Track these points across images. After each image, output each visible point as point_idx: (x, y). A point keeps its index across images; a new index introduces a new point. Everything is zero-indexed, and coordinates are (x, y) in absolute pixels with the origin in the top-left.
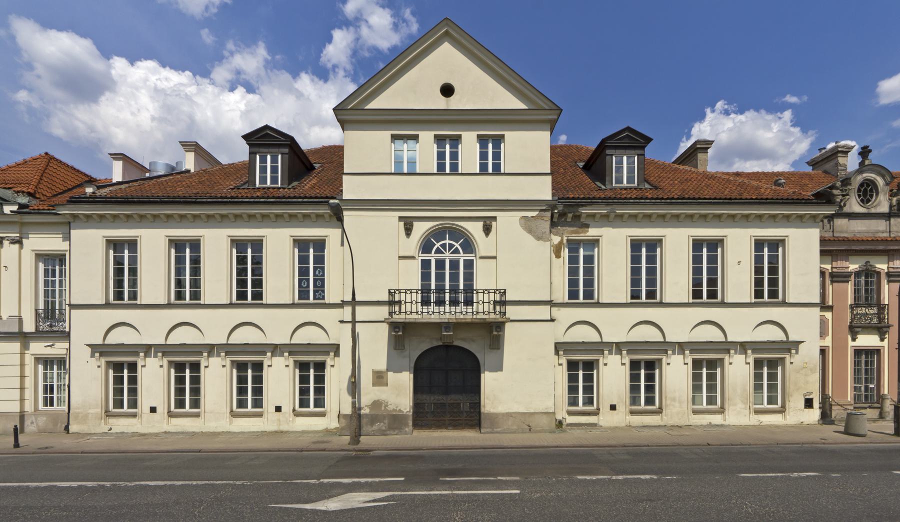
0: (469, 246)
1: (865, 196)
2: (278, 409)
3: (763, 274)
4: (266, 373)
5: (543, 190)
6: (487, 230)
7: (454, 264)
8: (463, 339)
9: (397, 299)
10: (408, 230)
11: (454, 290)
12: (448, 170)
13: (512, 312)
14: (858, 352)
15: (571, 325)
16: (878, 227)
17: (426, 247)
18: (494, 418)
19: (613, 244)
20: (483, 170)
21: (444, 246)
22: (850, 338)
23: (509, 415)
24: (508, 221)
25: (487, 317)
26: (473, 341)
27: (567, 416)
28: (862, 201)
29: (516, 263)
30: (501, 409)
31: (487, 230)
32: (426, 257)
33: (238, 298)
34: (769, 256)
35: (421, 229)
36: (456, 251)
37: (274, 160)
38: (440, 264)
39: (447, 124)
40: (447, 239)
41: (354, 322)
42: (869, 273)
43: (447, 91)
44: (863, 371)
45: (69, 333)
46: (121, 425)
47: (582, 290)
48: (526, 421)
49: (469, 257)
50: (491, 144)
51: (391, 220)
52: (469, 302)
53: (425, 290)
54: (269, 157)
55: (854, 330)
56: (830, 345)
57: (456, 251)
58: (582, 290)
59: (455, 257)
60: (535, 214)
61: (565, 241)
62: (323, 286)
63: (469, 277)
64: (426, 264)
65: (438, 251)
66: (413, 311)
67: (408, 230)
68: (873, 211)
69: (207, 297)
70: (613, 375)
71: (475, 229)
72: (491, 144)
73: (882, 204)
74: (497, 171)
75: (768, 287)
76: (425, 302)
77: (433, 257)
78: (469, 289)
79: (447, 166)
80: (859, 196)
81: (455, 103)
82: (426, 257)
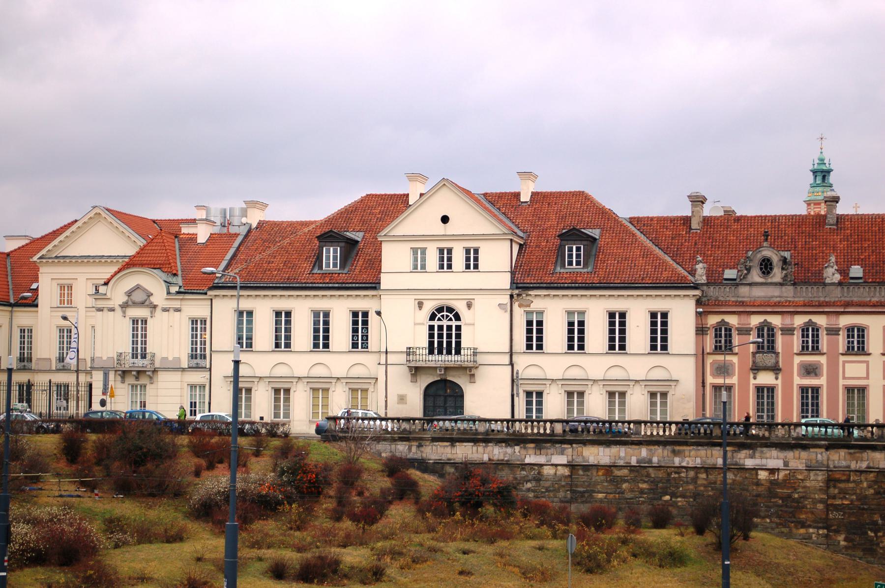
0: (457, 317)
1: (766, 268)
3: (578, 337)
5: (505, 281)
6: (469, 306)
10: (420, 305)
14: (760, 389)
16: (773, 293)
17: (433, 317)
19: (555, 310)
21: (443, 316)
22: (752, 376)
24: (480, 301)
28: (764, 273)
29: (487, 328)
31: (469, 306)
32: (432, 323)
34: (659, 325)
38: (440, 328)
41: (386, 364)
42: (767, 333)
44: (765, 403)
45: (210, 369)
46: (576, 304)
49: (458, 323)
52: (458, 352)
55: (756, 369)
56: (736, 382)
57: (451, 320)
59: (450, 323)
62: (367, 340)
64: (431, 328)
65: (439, 319)
66: (423, 358)
67: (420, 305)
68: (770, 281)
73: (777, 275)
75: (659, 340)
76: (431, 352)
77: (436, 323)
78: (458, 344)
80: (761, 269)
81: (451, 229)
82: (432, 323)
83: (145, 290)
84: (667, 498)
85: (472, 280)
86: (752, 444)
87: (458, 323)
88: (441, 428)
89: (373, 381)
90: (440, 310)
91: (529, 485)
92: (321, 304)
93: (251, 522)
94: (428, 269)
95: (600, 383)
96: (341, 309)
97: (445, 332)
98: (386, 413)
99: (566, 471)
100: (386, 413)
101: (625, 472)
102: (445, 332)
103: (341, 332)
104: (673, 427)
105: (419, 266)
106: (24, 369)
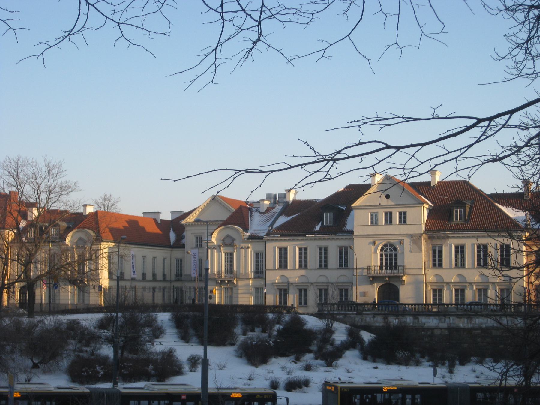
0: (395, 249)
38: (391, 255)
49: (395, 253)
52: (396, 268)
57: (392, 251)
59: (391, 253)
65: (385, 251)
76: (381, 268)
78: (396, 264)
83: (231, 237)
84: (502, 346)
85: (404, 229)
86: (477, 314)
87: (395, 253)
88: (492, 310)
89: (351, 285)
90: (385, 245)
91: (426, 340)
92: (283, 244)
93: (300, 358)
95: (295, 285)
96: (333, 245)
97: (391, 256)
98: (154, 300)
99: (446, 332)
100: (154, 300)
101: (479, 331)
102: (391, 256)
103: (333, 259)
104: (336, 306)
105: (374, 222)
106: (178, 280)
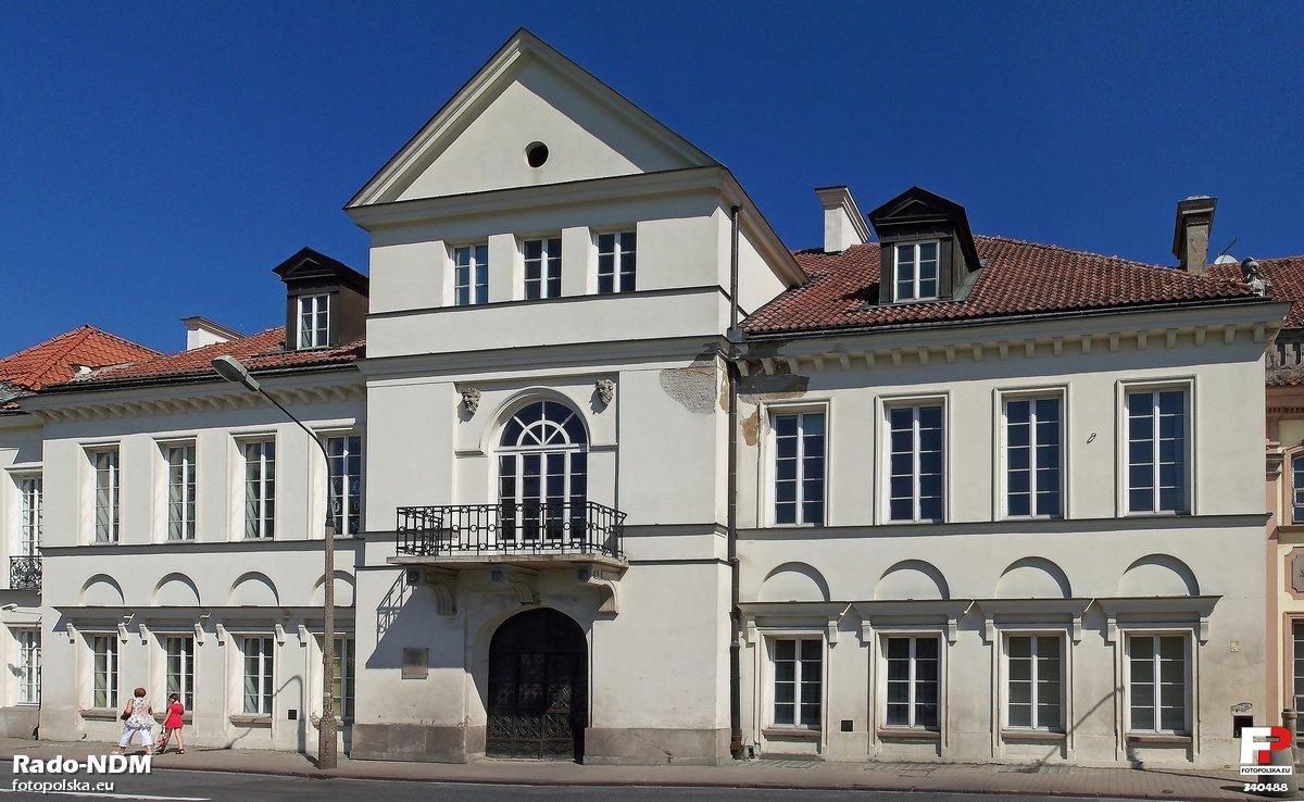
0: (578, 431)
2: (847, 726)
4: (830, 658)
7: (556, 462)
8: (559, 597)
9: (446, 525)
11: (531, 507)
12: (617, 288)
13: (631, 546)
15: (767, 573)
18: (606, 736)
20: (533, 295)
21: (537, 431)
23: (631, 733)
25: (518, 553)
26: (575, 599)
27: (763, 741)
29: (669, 454)
30: (622, 722)
32: (508, 451)
33: (780, 519)
34: (1161, 424)
35: (491, 403)
36: (559, 439)
37: (322, 306)
38: (532, 463)
39: (537, 217)
40: (547, 420)
43: (538, 155)
47: (804, 501)
48: (660, 741)
50: (618, 243)
51: (443, 391)
52: (578, 530)
53: (507, 507)
54: (315, 302)
57: (559, 439)
58: (804, 501)
60: (686, 364)
61: (763, 412)
63: (580, 484)
64: (507, 465)
65: (528, 440)
69: (957, 508)
70: (855, 672)
71: (580, 396)
72: (618, 243)
74: (483, 302)
75: (1163, 481)
76: (507, 531)
78: (579, 505)
79: (475, 297)
81: (549, 174)
94: (278, 537)
